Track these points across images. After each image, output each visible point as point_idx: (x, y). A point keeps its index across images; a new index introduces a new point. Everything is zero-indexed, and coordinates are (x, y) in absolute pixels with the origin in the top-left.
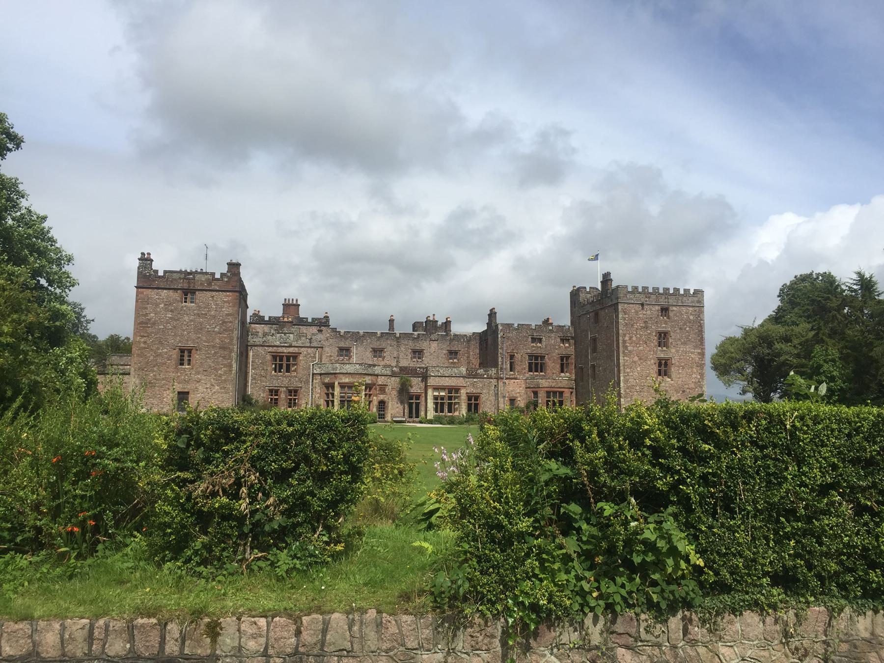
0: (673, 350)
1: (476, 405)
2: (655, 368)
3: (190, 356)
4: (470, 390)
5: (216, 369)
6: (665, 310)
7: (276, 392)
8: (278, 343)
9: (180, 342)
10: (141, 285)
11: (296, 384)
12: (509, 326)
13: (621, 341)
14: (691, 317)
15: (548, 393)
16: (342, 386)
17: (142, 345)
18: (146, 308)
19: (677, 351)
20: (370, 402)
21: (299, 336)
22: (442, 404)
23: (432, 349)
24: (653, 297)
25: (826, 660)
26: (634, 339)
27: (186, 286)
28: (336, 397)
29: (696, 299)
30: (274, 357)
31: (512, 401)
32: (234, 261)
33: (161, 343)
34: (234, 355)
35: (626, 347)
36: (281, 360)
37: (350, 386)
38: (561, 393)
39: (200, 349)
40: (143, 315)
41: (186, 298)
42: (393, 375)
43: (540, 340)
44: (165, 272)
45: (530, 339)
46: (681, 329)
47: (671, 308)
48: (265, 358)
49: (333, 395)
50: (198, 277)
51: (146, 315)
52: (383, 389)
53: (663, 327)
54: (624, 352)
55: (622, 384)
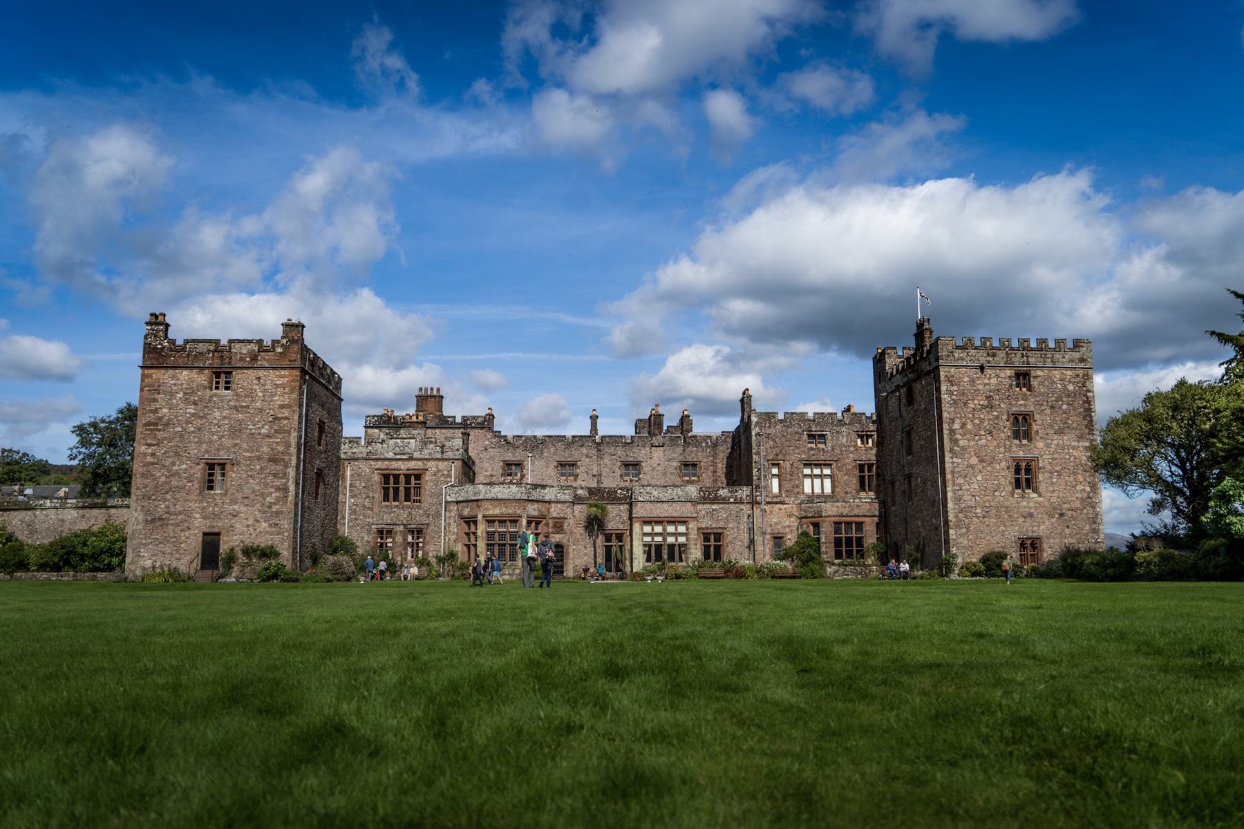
0: (1040, 444)
1: (718, 549)
2: (1010, 476)
3: (223, 475)
4: (706, 523)
5: (263, 495)
6: (1023, 377)
8: (391, 455)
9: (207, 452)
10: (148, 363)
12: (769, 417)
13: (946, 432)
14: (1071, 387)
16: (490, 521)
17: (149, 459)
18: (155, 400)
19: (1048, 446)
21: (425, 443)
23: (655, 461)
24: (1001, 354)
25: (1241, 377)
26: (970, 426)
27: (217, 362)
28: (479, 540)
29: (1077, 355)
30: (386, 477)
32: (294, 321)
33: (177, 454)
34: (291, 472)
38: (859, 526)
41: (217, 383)
42: (577, 500)
45: (805, 437)
46: (1052, 407)
47: (1033, 373)
48: (369, 479)
50: (236, 348)
51: (156, 411)
52: (559, 525)
53: (1020, 406)
54: (951, 450)
55: (950, 505)
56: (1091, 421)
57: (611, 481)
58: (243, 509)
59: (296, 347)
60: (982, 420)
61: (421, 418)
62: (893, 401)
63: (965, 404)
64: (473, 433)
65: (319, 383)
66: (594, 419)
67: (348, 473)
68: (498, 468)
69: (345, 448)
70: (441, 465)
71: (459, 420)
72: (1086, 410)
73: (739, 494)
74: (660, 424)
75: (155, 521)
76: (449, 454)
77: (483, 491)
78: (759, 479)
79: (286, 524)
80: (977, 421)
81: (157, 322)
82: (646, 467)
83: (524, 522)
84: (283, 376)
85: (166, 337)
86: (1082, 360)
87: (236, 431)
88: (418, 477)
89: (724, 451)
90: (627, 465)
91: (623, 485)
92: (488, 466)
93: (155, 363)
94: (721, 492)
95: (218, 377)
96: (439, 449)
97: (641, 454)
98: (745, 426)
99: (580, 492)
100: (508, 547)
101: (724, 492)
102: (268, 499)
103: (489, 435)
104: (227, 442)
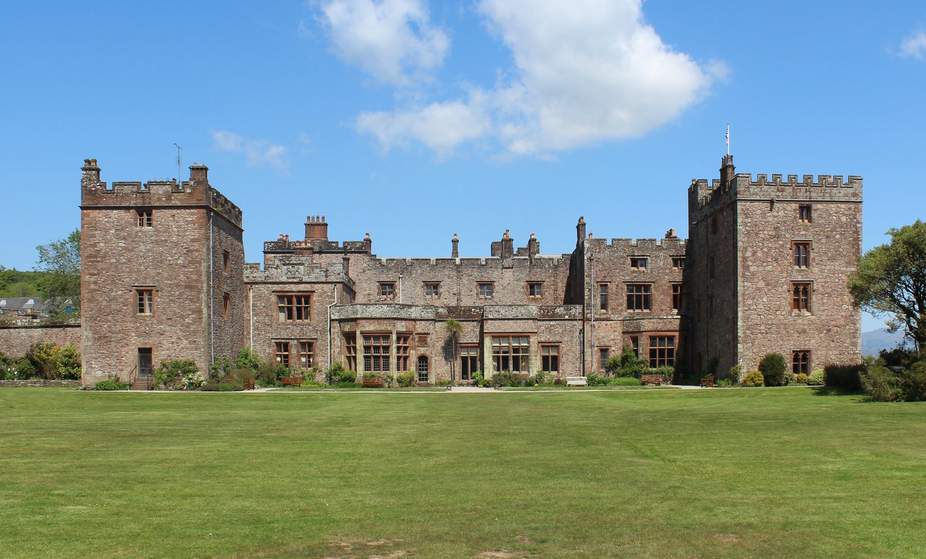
0: (816, 270)
2: (789, 297)
3: (150, 300)
5: (182, 317)
6: (805, 210)
7: (286, 347)
8: (284, 279)
9: (137, 280)
10: (86, 204)
11: (310, 334)
12: (600, 242)
13: (739, 259)
14: (844, 219)
15: (652, 338)
16: (367, 336)
17: (93, 286)
18: (94, 236)
19: (822, 271)
20: (406, 358)
21: (312, 268)
22: (506, 359)
23: (505, 281)
24: (789, 190)
26: (759, 254)
27: (139, 203)
28: (358, 352)
29: (850, 191)
31: (604, 351)
34: (203, 296)
35: (746, 268)
36: (290, 302)
37: (376, 336)
39: (162, 290)
40: (91, 246)
43: (644, 262)
44: (115, 185)
45: (629, 262)
46: (828, 237)
47: (814, 206)
49: (355, 348)
51: (94, 245)
52: (423, 338)
55: (740, 323)
56: (859, 249)
57: (468, 301)
58: (168, 328)
59: (202, 188)
60: (770, 249)
61: (309, 245)
62: (702, 229)
63: (757, 234)
64: (353, 257)
65: (224, 217)
66: (455, 242)
67: (251, 294)
68: (375, 287)
69: (247, 273)
70: (327, 287)
71: (341, 245)
72: (854, 240)
73: (573, 311)
74: (510, 249)
75: (102, 339)
76: (332, 278)
77: (361, 312)
78: (590, 298)
79: (201, 341)
80: (765, 250)
81: (91, 168)
82: (497, 287)
83: (394, 337)
84: (192, 214)
85: (98, 181)
86: (855, 195)
87: (159, 261)
88: (307, 299)
89: (563, 275)
90: (482, 284)
91: (478, 304)
92: (366, 288)
93: (92, 204)
94: (558, 310)
95: (141, 215)
96: (323, 273)
97: (493, 275)
98: (580, 249)
99: (440, 310)
100: (382, 359)
101: (560, 310)
102: (187, 320)
103: (367, 258)
104: (152, 272)
